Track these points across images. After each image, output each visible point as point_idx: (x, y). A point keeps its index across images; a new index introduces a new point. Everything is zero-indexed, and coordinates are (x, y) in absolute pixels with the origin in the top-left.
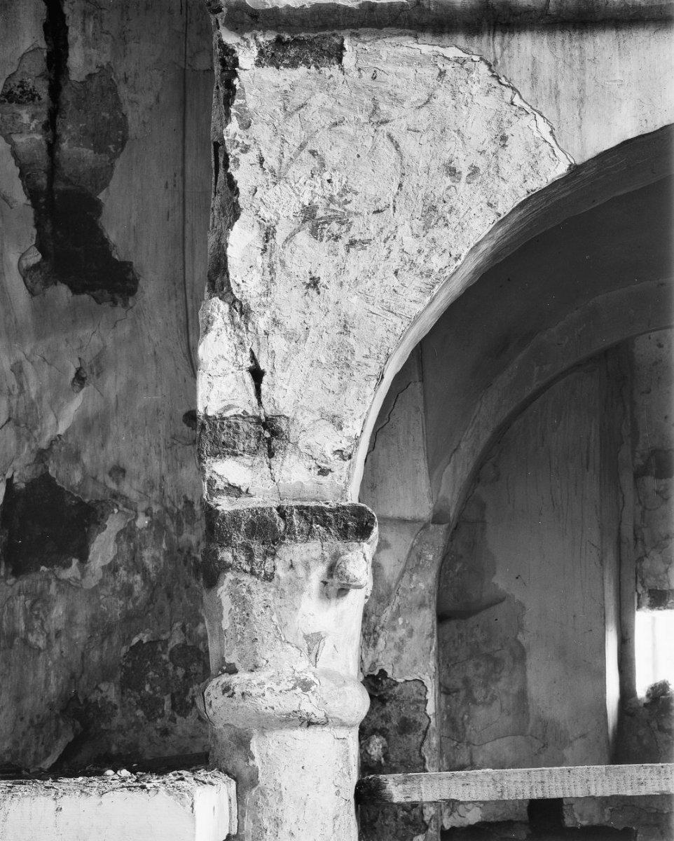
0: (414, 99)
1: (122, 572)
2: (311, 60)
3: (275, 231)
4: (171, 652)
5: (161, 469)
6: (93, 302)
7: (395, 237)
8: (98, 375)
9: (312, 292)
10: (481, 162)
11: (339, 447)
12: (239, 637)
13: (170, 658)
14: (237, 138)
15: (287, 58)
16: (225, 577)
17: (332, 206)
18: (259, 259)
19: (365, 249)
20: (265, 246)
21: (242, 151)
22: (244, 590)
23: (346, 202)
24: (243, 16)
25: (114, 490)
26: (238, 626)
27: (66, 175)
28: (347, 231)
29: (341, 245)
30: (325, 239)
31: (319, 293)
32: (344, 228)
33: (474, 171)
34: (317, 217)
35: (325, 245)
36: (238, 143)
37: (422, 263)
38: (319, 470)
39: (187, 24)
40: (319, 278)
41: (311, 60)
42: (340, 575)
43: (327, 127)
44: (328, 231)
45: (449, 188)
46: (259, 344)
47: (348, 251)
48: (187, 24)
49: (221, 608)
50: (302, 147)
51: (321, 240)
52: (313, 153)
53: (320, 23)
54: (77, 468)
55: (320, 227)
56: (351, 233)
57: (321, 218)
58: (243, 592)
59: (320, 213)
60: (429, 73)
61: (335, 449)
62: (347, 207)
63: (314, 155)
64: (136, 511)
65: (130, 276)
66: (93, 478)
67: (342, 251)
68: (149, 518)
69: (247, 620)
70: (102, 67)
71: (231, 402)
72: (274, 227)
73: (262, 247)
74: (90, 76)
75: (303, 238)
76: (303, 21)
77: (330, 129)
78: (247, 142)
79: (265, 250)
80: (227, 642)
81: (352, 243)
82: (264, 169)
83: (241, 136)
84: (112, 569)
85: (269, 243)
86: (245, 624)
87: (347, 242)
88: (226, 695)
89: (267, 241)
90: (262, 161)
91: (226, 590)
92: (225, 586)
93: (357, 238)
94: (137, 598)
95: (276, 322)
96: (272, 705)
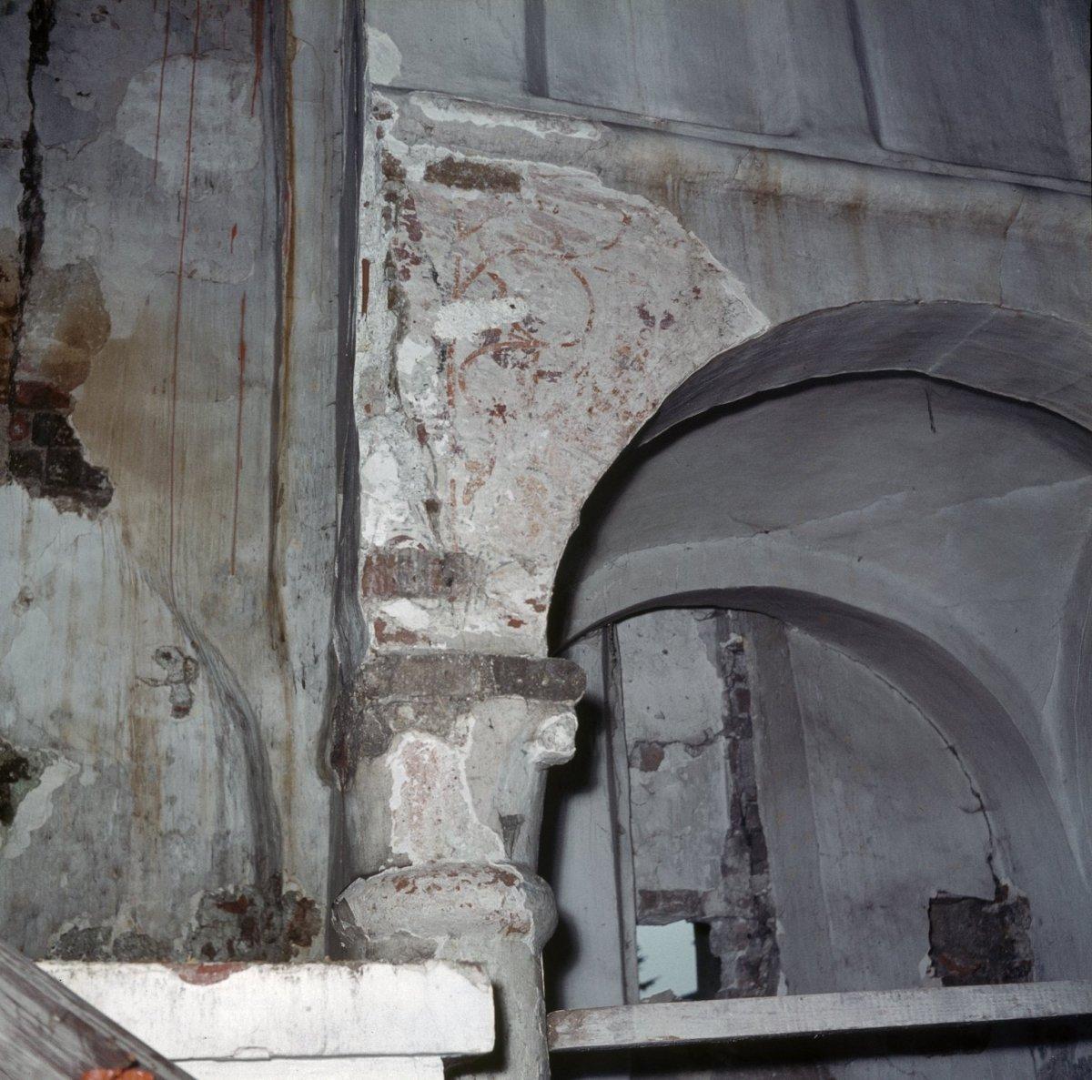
0: (599, 238)
1: (57, 840)
2: (486, 185)
3: (452, 351)
4: (116, 943)
5: (118, 713)
6: (54, 510)
7: (587, 373)
8: (48, 597)
9: (498, 420)
10: (675, 310)
11: (531, 596)
12: (415, 818)
13: (114, 951)
14: (407, 248)
15: (460, 179)
16: (402, 739)
17: (516, 332)
18: (435, 379)
19: (553, 380)
20: (441, 365)
21: (412, 262)
22: (426, 757)
23: (532, 331)
24: (415, 126)
25: (55, 737)
26: (415, 804)
27: (33, 366)
28: (533, 361)
29: (528, 374)
30: (510, 366)
31: (505, 422)
32: (531, 357)
33: (668, 319)
34: (500, 342)
35: (510, 373)
36: (407, 254)
37: (618, 404)
38: (509, 620)
39: (184, 231)
40: (505, 406)
41: (486, 185)
42: (547, 742)
43: (506, 253)
44: (513, 358)
45: (644, 330)
46: (435, 471)
47: (536, 382)
48: (184, 231)
49: (390, 781)
50: (480, 268)
51: (506, 366)
52: (493, 276)
53: (499, 149)
54: (9, 709)
55: (503, 353)
56: (540, 362)
57: (504, 344)
58: (424, 760)
59: (503, 339)
60: (614, 217)
61: (528, 597)
62: (533, 335)
63: (494, 279)
64: (81, 765)
65: (103, 485)
66: (29, 721)
67: (529, 381)
68: (97, 774)
69: (429, 795)
70: (83, 260)
71: (405, 533)
72: (450, 345)
73: (437, 365)
74: (69, 267)
75: (486, 361)
76: (481, 142)
77: (509, 254)
78: (417, 254)
79: (441, 369)
80: (396, 826)
81: (540, 374)
82: (438, 284)
83: (410, 247)
84: (45, 836)
85: (446, 363)
86: (424, 801)
87: (534, 372)
88: (403, 891)
89: (443, 360)
90: (435, 275)
91: (399, 758)
92: (399, 752)
93: (546, 369)
94: (74, 874)
95: (456, 450)
96: (469, 901)
